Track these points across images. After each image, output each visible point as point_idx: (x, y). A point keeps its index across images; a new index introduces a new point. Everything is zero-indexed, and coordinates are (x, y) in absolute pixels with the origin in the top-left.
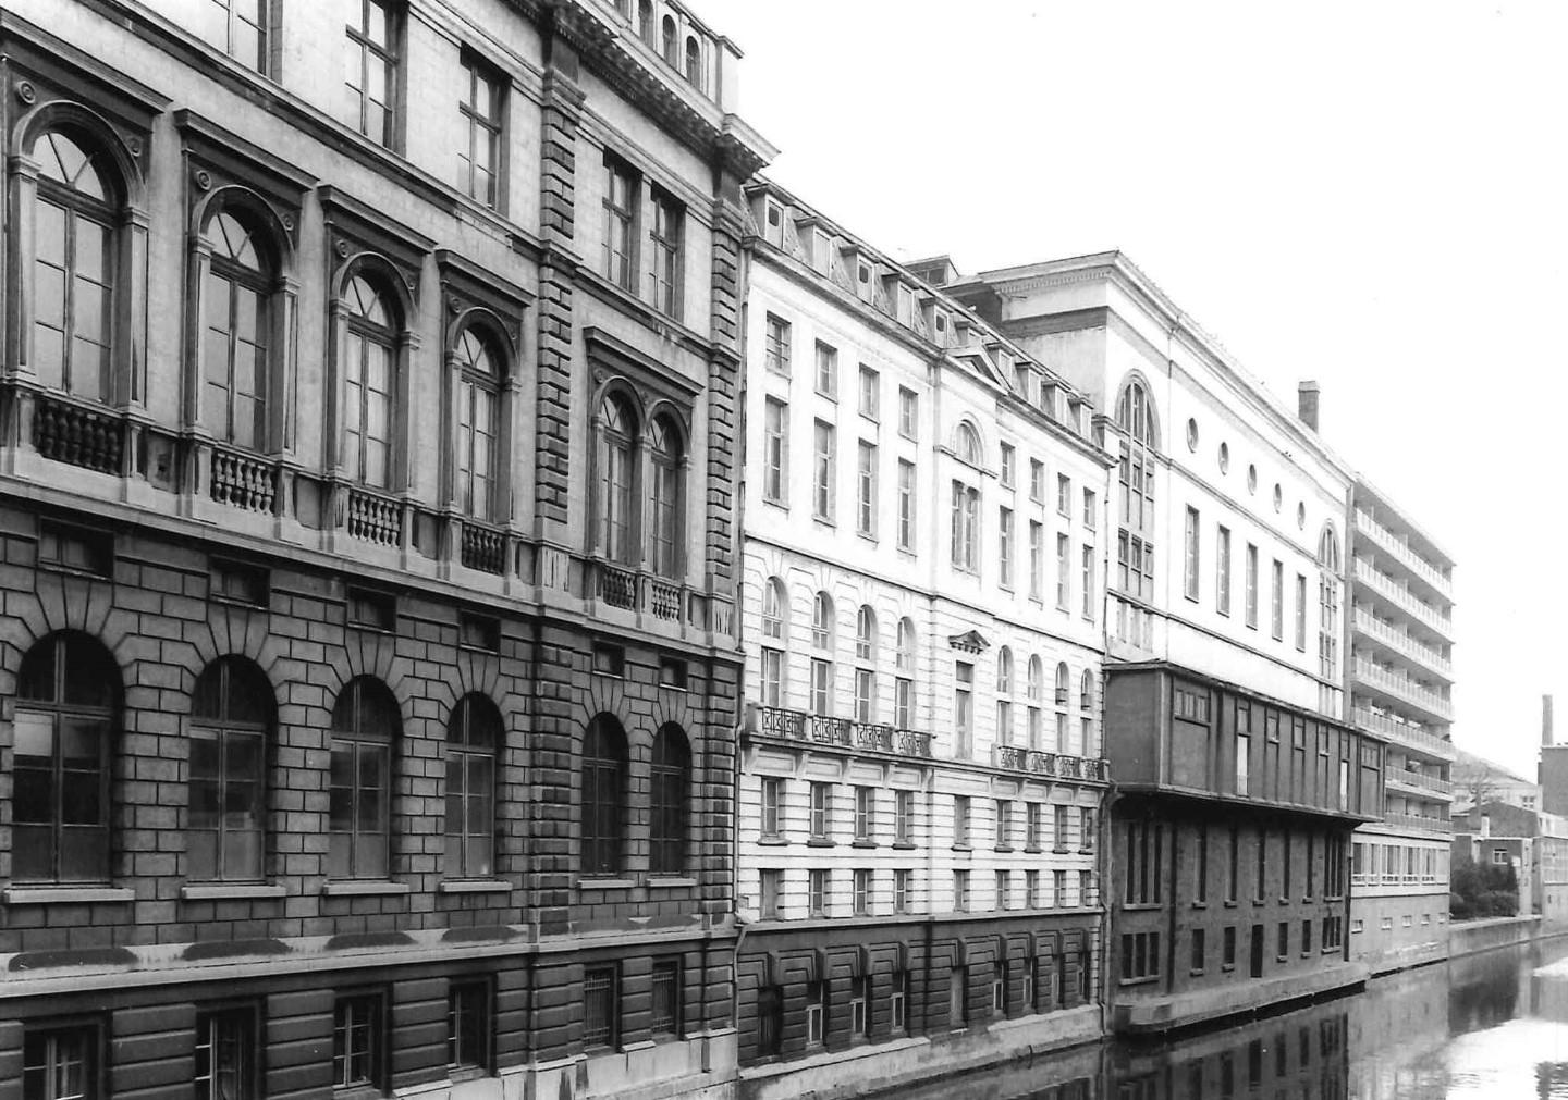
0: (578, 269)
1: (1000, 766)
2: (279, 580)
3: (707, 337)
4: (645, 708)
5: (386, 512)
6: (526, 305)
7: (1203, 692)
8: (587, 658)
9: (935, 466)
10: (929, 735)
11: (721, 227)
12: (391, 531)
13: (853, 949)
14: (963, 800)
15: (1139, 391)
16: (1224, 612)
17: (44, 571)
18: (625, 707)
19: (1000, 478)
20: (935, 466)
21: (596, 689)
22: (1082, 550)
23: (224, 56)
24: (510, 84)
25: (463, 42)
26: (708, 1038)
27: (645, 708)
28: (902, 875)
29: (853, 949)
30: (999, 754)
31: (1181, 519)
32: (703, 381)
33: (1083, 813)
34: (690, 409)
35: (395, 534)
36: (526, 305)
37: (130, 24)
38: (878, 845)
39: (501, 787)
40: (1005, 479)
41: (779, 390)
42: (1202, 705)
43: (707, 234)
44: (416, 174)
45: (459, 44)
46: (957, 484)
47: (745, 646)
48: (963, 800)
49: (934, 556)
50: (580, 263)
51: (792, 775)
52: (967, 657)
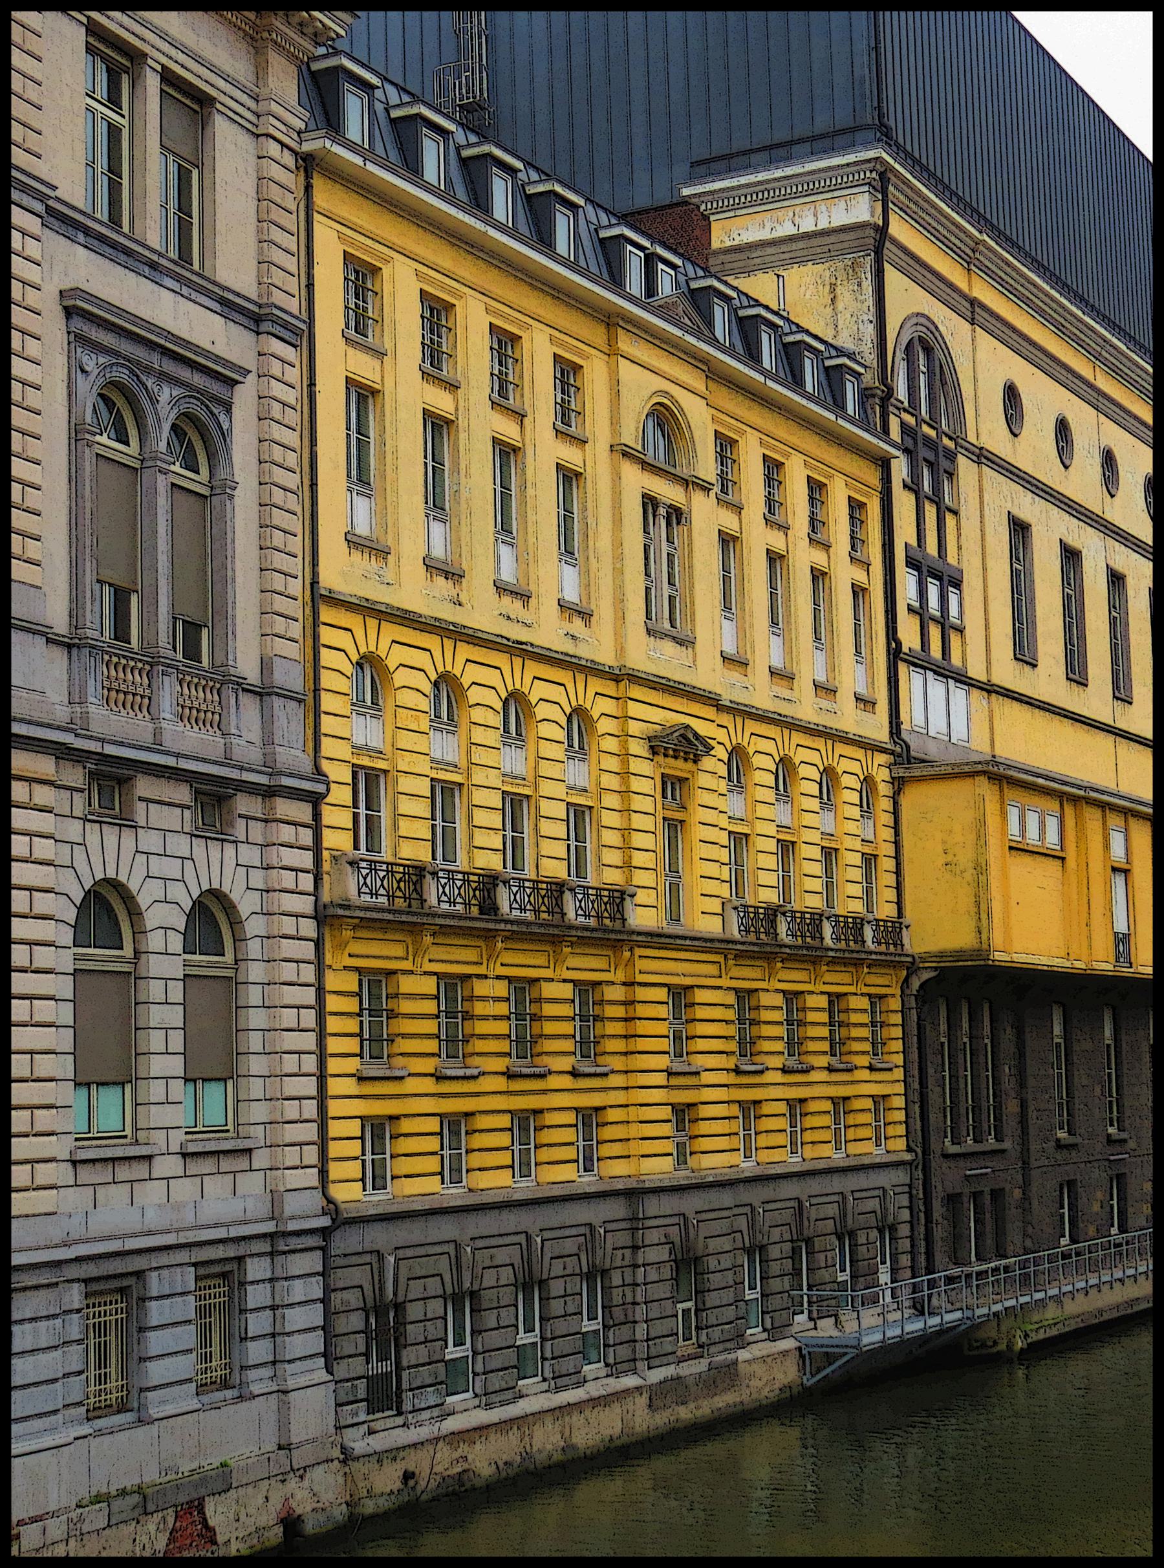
0: (51, 203)
1: (736, 935)
2: (144, 786)
3: (254, 297)
4: (171, 868)
5: (200, 689)
6: (237, 382)
7: (1054, 805)
8: (187, 813)
9: (617, 477)
10: (623, 893)
11: (272, 131)
12: (142, 697)
13: (515, 1239)
14: (680, 995)
15: (928, 350)
16: (1076, 673)
17: (89, 821)
18: (139, 872)
19: (716, 489)
20: (617, 477)
21: (93, 838)
22: (809, 577)
23: (160, 254)
24: (213, 106)
25: (163, 65)
26: (286, 1392)
27: (171, 868)
28: (589, 1118)
29: (515, 1239)
30: (733, 918)
31: (999, 539)
32: (248, 360)
33: (788, 1001)
34: (228, 407)
35: (146, 701)
36: (237, 382)
37: (81, 237)
38: (813, 1068)
39: (242, 1012)
40: (724, 490)
41: (365, 368)
42: (1052, 824)
43: (245, 140)
44: (231, 297)
45: (159, 68)
46: (650, 502)
47: (326, 766)
48: (680, 995)
49: (621, 617)
50: (52, 194)
51: (406, 965)
52: (678, 767)
